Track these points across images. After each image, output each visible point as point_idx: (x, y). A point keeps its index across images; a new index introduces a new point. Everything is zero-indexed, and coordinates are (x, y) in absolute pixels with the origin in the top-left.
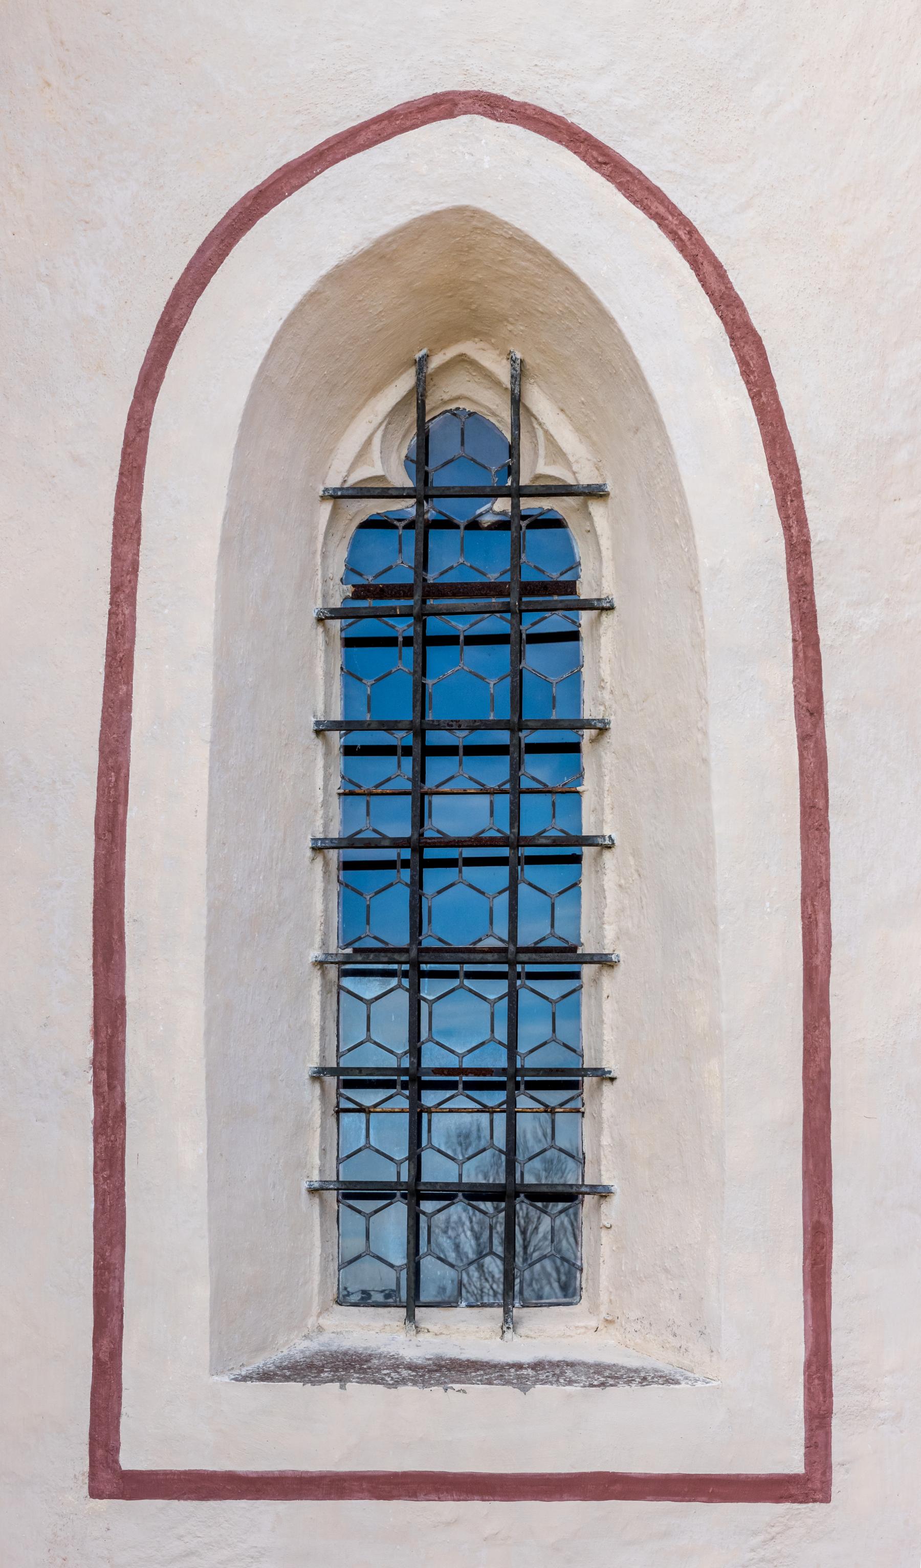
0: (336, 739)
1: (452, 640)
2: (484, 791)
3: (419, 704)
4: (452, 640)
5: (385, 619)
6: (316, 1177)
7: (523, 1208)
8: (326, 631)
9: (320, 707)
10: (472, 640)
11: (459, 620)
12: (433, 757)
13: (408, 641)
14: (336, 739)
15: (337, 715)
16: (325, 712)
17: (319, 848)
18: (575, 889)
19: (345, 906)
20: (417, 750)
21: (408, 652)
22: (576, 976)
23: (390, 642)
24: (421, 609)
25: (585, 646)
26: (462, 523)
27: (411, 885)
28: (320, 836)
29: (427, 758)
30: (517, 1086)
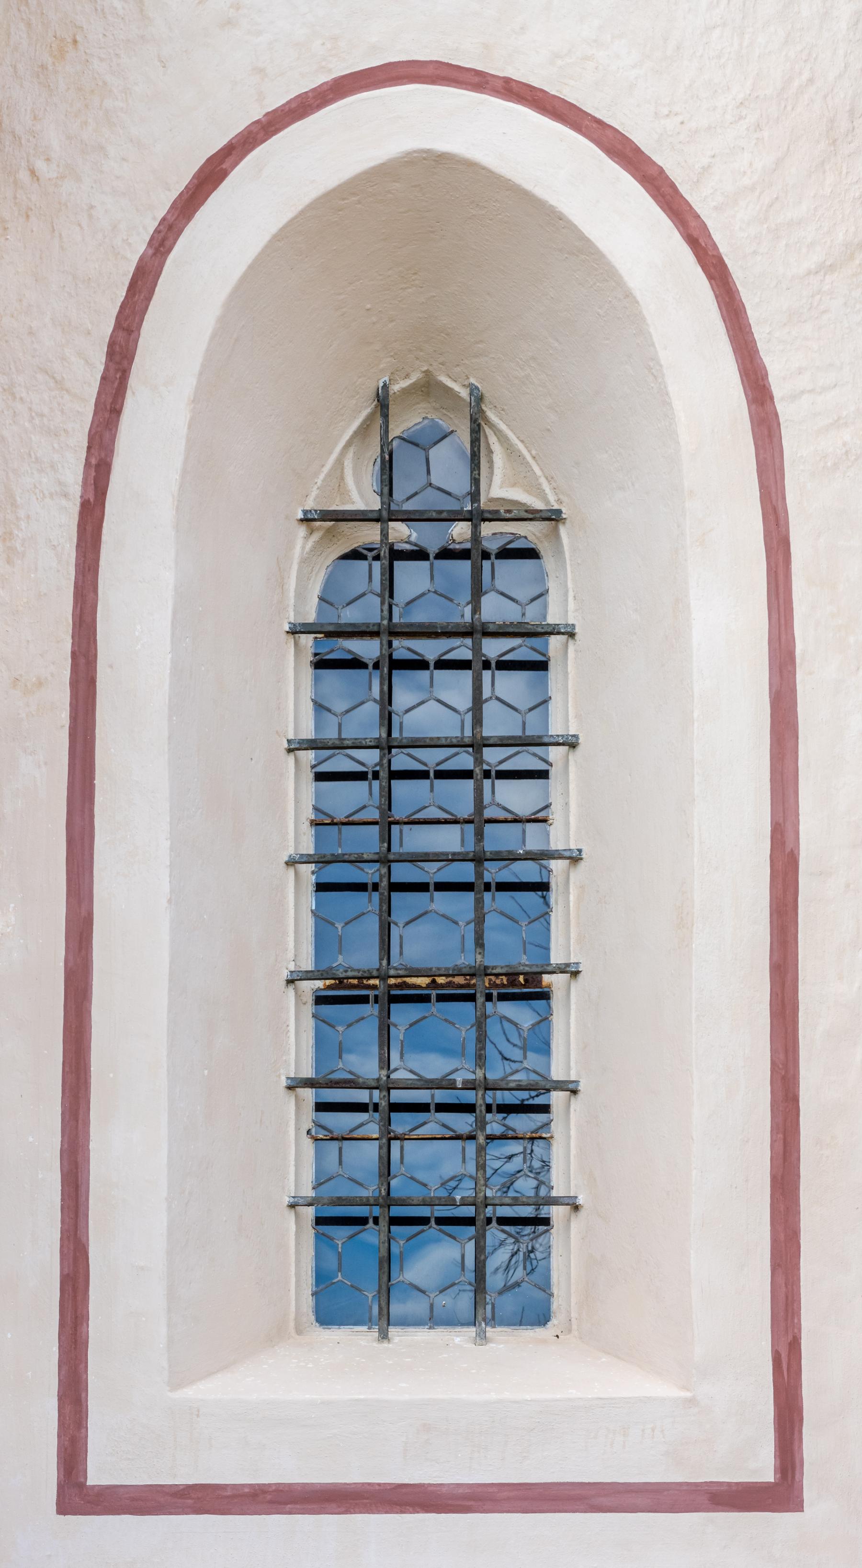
0: (310, 1212)
1: (420, 664)
2: (458, 1137)
3: (387, 682)
4: (420, 664)
5: (349, 751)
6: (291, 851)
7: (494, 1234)
8: (297, 1216)
9: (292, 1188)
10: (442, 887)
11: (430, 614)
12: (403, 672)
13: (376, 887)
14: (309, 1095)
15: (308, 1072)
16: (296, 1070)
17: (293, 1086)
18: (546, 1021)
19: (320, 1042)
20: (384, 774)
21: (376, 896)
22: (545, 1109)
23: (360, 887)
24: (388, 741)
25: (556, 1235)
26: (433, 550)
27: (381, 703)
28: (292, 1076)
29: (394, 671)
30: (489, 1221)
